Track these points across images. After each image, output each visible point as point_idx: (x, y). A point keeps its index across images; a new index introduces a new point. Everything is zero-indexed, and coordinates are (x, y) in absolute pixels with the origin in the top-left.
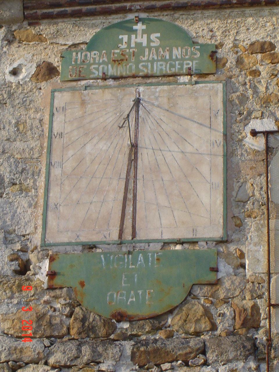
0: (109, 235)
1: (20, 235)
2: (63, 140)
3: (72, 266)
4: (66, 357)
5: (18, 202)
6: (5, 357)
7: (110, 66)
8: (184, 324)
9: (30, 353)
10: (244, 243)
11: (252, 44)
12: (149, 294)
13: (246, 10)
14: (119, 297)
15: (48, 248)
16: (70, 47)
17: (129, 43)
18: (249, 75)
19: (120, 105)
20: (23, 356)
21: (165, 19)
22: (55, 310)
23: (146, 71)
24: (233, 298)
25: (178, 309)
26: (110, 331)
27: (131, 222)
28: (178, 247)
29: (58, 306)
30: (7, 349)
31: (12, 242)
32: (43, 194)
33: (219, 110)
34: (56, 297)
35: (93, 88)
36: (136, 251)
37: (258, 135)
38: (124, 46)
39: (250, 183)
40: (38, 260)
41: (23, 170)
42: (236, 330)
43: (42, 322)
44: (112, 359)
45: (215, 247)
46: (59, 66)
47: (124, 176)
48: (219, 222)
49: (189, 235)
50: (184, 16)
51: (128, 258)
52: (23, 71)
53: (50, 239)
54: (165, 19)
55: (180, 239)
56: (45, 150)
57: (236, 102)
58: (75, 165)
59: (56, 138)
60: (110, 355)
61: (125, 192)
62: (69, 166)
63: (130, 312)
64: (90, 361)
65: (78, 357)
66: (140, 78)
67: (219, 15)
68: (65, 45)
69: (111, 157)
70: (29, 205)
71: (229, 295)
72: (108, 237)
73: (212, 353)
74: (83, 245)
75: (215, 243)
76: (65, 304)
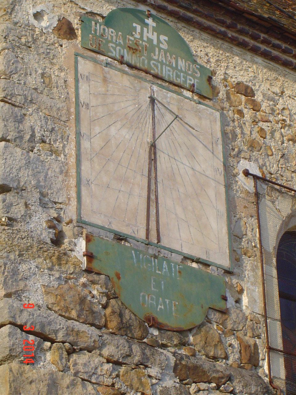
0: (137, 231)
1: (52, 201)
2: (90, 112)
3: (107, 254)
4: (119, 353)
5: (49, 162)
6: (62, 337)
7: (125, 50)
8: (205, 346)
9: (87, 339)
10: (243, 279)
11: (238, 84)
12: (175, 305)
13: (234, 48)
14: (150, 301)
15: (83, 226)
16: (87, 13)
17: (142, 33)
18: (236, 113)
19: (138, 97)
20: (80, 340)
21: (170, 24)
22: (93, 297)
23: (156, 71)
24: (238, 331)
25: (196, 328)
26: (145, 334)
27: (156, 224)
28: (194, 265)
29: (95, 292)
30: (65, 328)
31: (46, 206)
32: (75, 164)
33: (218, 139)
34: (93, 282)
35: (113, 68)
36: (160, 256)
37: (249, 176)
38: (138, 36)
39: (244, 221)
40: (74, 236)
41: (53, 129)
42: (242, 364)
43: (83, 306)
44: (159, 366)
45: (222, 275)
46: (78, 29)
47: (146, 173)
48: (226, 252)
49: (203, 257)
50: (185, 29)
51: (154, 261)
52: (44, 19)
53: (85, 217)
54: (170, 24)
55: (200, 258)
56: (73, 116)
57: (229, 136)
58: (102, 144)
59: (83, 107)
60: (158, 361)
61: (148, 191)
62: (98, 143)
63: (161, 320)
64: (140, 363)
65: (129, 356)
66: (151, 76)
67: (213, 42)
68: (83, 9)
69: (133, 148)
70: (60, 170)
71: (235, 327)
72: (136, 233)
73: (238, 383)
74: (115, 234)
75: (223, 271)
76: (103, 293)
